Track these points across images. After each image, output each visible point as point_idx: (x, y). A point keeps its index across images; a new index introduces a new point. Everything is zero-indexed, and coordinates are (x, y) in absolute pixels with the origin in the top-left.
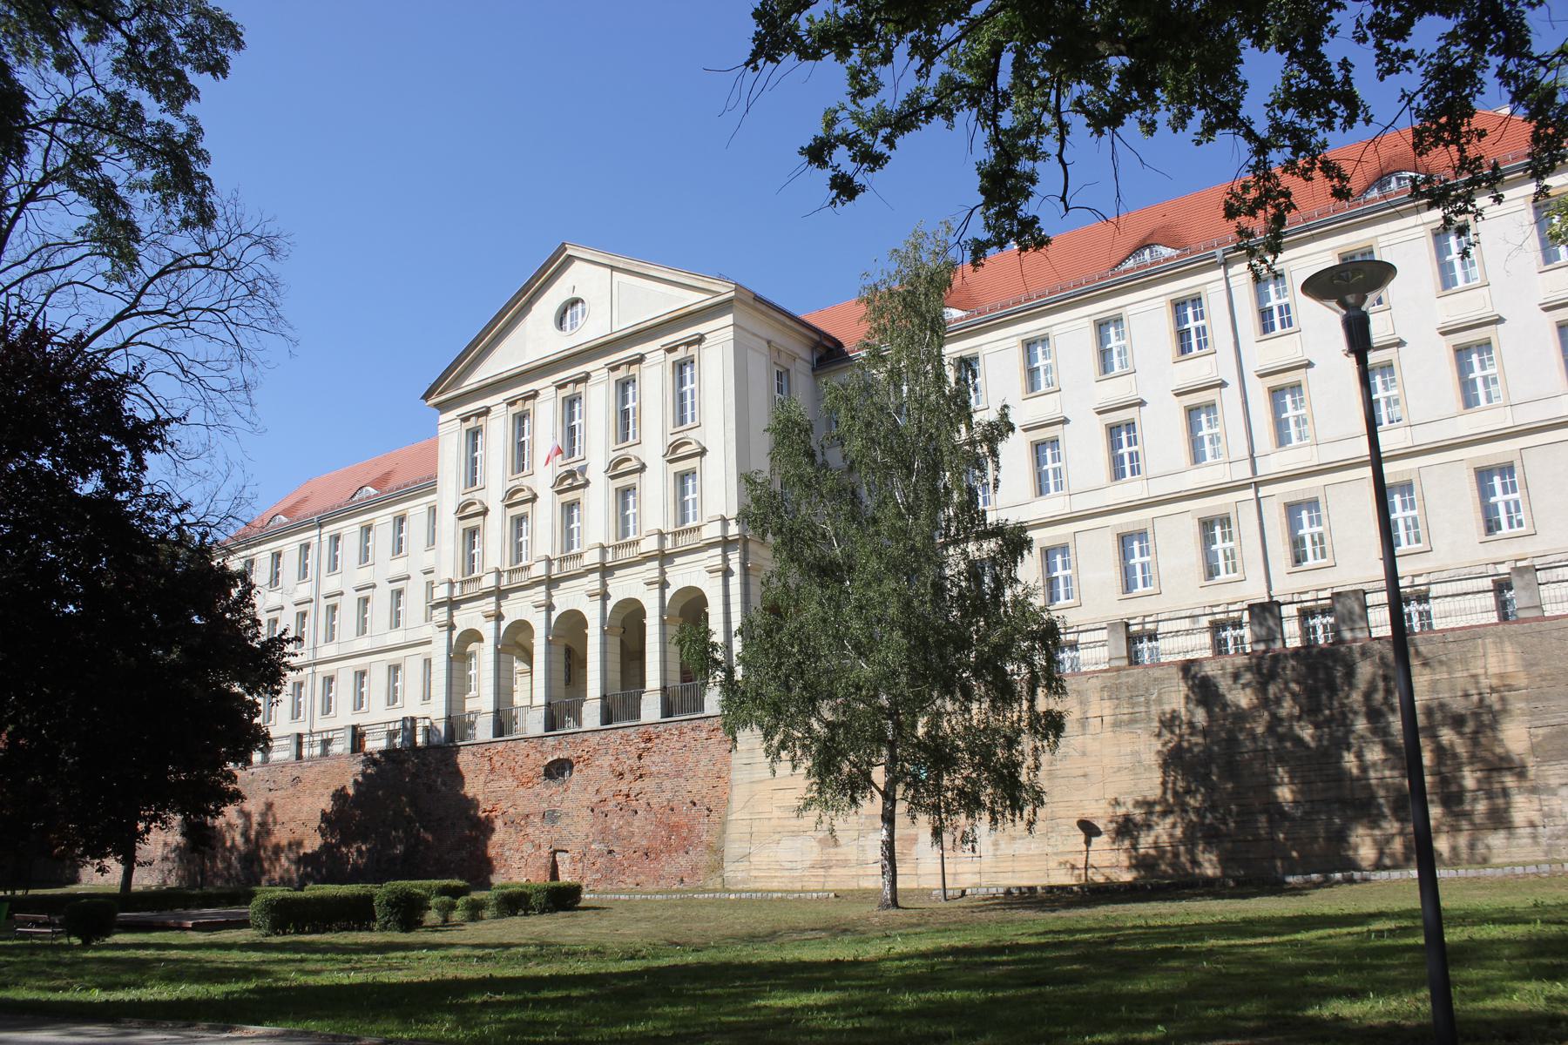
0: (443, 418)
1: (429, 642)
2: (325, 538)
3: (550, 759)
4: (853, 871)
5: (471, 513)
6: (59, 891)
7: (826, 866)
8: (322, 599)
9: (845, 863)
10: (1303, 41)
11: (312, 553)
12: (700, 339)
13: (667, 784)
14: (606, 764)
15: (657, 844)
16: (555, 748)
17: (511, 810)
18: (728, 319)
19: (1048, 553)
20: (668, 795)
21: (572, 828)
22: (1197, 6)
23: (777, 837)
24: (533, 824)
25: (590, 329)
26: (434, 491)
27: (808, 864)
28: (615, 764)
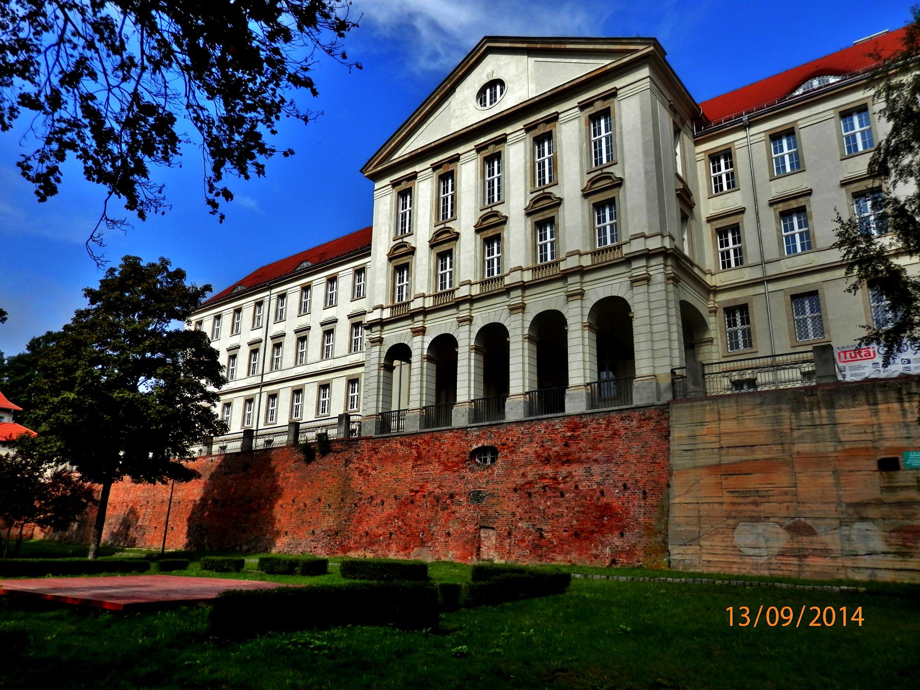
0: (377, 185)
1: (363, 365)
2: (274, 296)
3: (475, 447)
4: (839, 562)
5: (401, 260)
6: (53, 560)
7: (801, 555)
8: (269, 338)
9: (825, 552)
10: (269, 14)
11: (265, 306)
12: (613, 94)
13: (596, 469)
14: (531, 451)
15: (589, 526)
16: (479, 437)
17: (437, 491)
18: (645, 72)
19: (853, 151)
20: (598, 479)
21: (498, 508)
22: (305, 4)
23: (731, 522)
24: (459, 504)
25: (509, 101)
26: (369, 255)
27: (776, 550)
28: (540, 451)
